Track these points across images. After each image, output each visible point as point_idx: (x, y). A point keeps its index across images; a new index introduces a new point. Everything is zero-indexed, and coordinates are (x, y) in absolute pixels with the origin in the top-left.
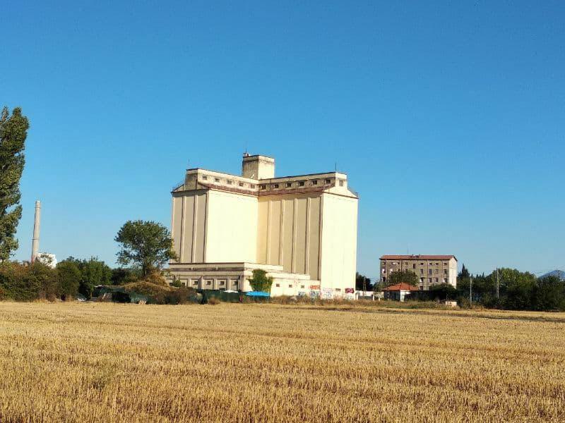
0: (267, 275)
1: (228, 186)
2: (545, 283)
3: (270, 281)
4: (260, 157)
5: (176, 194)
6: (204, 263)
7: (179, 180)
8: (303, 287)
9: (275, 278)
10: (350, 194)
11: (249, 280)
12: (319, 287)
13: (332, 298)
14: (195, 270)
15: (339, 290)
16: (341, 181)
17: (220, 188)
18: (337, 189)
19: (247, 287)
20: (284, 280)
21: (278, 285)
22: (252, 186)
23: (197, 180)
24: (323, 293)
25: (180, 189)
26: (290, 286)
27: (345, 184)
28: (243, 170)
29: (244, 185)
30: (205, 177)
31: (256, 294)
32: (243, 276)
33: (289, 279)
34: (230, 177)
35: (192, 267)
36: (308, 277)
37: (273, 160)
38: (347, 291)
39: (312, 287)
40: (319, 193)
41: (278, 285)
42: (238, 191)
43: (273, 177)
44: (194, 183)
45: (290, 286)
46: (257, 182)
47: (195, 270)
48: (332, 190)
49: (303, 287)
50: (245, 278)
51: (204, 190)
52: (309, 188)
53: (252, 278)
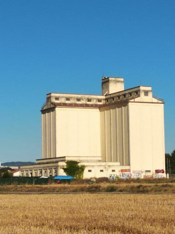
0: (79, 164)
1: (67, 102)
2: (68, 173)
3: (83, 168)
4: (110, 79)
5: (44, 112)
6: (56, 158)
7: (42, 103)
8: (113, 171)
9: (86, 166)
10: (155, 100)
11: (63, 169)
12: (129, 170)
13: (142, 177)
14: (39, 164)
15: (149, 171)
16: (146, 93)
17: (65, 105)
18: (142, 97)
19: (62, 173)
20: (95, 167)
21: (90, 171)
22: (99, 100)
23: (51, 102)
24: (133, 175)
25: (45, 108)
26: (102, 171)
27: (150, 94)
28: (102, 89)
29: (92, 101)
30: (57, 99)
31: (70, 178)
32: (58, 166)
33: (100, 166)
34: (79, 96)
35: (45, 161)
36: (118, 163)
37: (122, 80)
38: (157, 171)
39: (122, 171)
40: (125, 103)
41: (90, 171)
42: (87, 106)
43: (123, 90)
44: (49, 103)
45: (102, 171)
46: (104, 97)
47: (43, 163)
48: (137, 100)
49: (113, 171)
50: (59, 168)
51: (55, 105)
52: (120, 102)
53: (65, 167)
